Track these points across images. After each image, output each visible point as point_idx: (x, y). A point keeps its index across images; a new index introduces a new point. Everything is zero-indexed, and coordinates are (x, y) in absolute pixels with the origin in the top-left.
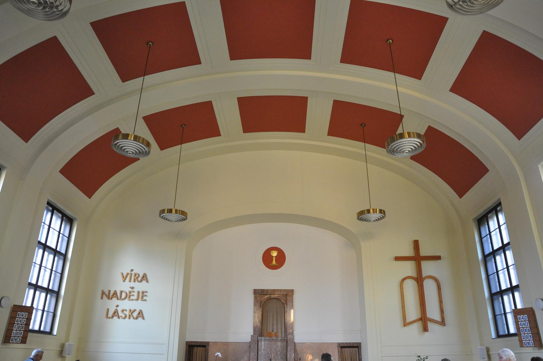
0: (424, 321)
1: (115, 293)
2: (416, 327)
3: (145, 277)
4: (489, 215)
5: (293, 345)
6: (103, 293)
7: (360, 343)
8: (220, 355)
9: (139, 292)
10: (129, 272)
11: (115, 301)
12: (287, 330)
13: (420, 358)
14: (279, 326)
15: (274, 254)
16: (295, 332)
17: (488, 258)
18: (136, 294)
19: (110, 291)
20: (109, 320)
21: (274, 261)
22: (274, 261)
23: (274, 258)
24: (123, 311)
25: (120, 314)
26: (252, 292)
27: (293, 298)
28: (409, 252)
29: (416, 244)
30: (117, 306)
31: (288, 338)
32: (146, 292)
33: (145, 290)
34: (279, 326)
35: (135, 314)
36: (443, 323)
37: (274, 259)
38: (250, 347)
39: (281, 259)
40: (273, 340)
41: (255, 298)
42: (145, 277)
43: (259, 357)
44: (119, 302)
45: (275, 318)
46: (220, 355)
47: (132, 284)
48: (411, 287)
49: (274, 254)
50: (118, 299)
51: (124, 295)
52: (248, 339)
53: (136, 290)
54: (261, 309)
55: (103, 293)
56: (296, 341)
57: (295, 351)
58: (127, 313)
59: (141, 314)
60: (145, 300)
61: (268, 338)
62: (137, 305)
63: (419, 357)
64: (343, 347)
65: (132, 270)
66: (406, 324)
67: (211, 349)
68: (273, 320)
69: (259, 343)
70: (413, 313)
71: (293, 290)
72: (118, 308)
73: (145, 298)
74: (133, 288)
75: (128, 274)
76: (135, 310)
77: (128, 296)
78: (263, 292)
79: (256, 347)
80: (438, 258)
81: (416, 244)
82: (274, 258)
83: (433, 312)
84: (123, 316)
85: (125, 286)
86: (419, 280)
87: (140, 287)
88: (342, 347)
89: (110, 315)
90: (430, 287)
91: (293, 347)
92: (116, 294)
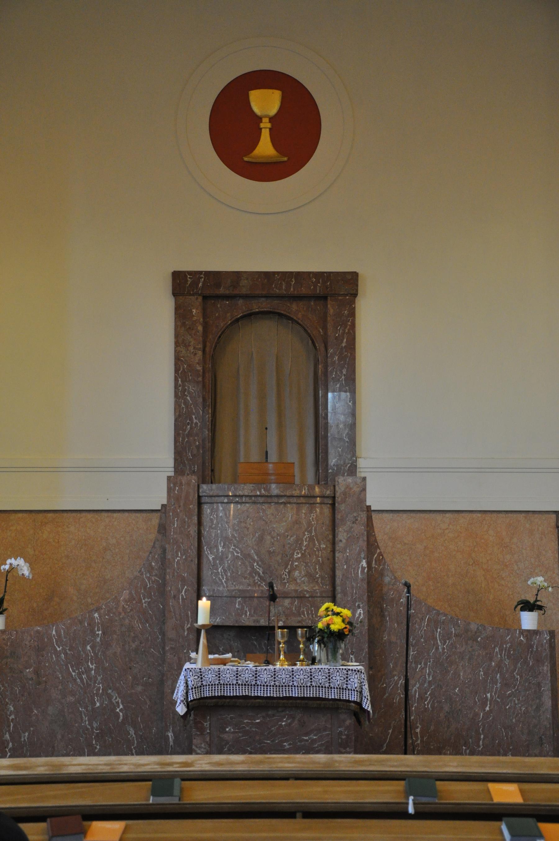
5: (364, 515)
8: (25, 570)
14: (292, 440)
15: (265, 103)
16: (361, 463)
21: (265, 136)
22: (265, 136)
23: (265, 125)
27: (352, 314)
31: (340, 489)
34: (292, 440)
37: (265, 130)
38: (163, 529)
40: (269, 498)
41: (181, 314)
43: (206, 573)
45: (272, 401)
46: (25, 570)
49: (265, 103)
52: (156, 496)
56: (375, 499)
57: (410, 722)
61: (246, 489)
68: (262, 397)
69: (207, 510)
71: (355, 275)
78: (218, 285)
79: (193, 530)
82: (265, 125)
91: (360, 529)
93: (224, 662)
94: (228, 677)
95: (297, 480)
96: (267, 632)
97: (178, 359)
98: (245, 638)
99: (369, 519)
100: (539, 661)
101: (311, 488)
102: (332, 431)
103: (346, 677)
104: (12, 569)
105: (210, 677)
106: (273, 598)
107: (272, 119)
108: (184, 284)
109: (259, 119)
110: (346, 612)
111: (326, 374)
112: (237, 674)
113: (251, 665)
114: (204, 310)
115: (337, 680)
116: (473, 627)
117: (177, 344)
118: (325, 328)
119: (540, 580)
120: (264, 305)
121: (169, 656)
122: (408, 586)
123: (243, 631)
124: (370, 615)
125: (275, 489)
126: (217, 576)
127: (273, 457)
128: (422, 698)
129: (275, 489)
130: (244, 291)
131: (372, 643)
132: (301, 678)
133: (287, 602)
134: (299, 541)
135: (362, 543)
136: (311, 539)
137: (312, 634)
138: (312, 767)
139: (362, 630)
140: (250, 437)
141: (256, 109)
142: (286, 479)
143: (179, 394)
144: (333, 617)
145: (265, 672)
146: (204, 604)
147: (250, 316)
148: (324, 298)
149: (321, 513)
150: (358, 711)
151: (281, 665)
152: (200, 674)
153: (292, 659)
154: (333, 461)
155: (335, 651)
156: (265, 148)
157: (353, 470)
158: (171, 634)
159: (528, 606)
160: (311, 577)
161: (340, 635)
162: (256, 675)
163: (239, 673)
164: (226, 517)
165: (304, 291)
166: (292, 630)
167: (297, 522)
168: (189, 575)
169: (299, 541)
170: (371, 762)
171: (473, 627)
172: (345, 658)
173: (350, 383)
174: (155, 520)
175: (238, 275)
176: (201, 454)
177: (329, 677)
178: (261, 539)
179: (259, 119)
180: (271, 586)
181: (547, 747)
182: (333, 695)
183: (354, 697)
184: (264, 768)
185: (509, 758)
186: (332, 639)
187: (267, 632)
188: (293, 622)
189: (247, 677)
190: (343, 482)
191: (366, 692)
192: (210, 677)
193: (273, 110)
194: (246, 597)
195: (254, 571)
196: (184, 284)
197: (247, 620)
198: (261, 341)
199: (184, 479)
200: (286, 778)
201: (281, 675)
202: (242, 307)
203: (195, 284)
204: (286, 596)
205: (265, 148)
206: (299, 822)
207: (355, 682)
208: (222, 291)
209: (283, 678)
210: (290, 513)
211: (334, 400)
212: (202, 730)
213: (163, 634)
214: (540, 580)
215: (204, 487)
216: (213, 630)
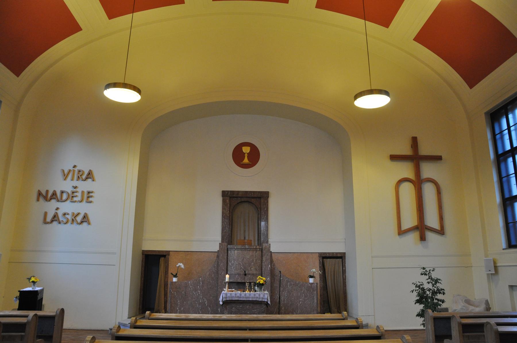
0: (421, 229)
1: (54, 194)
2: (415, 236)
3: (90, 175)
4: (509, 107)
6: (40, 194)
7: (344, 254)
8: (183, 266)
9: (83, 192)
10: (72, 168)
11: (54, 204)
12: (261, 239)
13: (424, 271)
15: (246, 150)
16: (269, 240)
17: (501, 158)
18: (79, 194)
19: (47, 191)
20: (47, 225)
23: (246, 155)
24: (65, 214)
25: (61, 218)
26: (221, 193)
27: (268, 202)
28: (406, 150)
29: (415, 141)
30: (57, 209)
31: (264, 247)
32: (92, 192)
33: (90, 190)
35: (79, 219)
36: (441, 232)
37: (246, 156)
38: (218, 257)
39: (255, 156)
40: (245, 249)
41: (224, 201)
42: (90, 175)
43: (229, 268)
44: (59, 205)
46: (183, 266)
47: (75, 183)
48: (408, 191)
49: (246, 150)
50: (58, 201)
51: (65, 196)
53: (79, 190)
54: (277, 272)
55: (40, 194)
56: (273, 249)
57: (272, 261)
58: (69, 217)
59: (85, 219)
60: (91, 202)
61: (239, 247)
62: (81, 208)
63: (424, 269)
64: (324, 257)
65: (75, 166)
66: (401, 232)
67: (172, 259)
69: (229, 252)
70: (410, 220)
71: (268, 192)
72: (58, 212)
73: (90, 199)
74: (75, 187)
75: (70, 171)
76: (78, 214)
77: (71, 197)
78: (234, 194)
79: (226, 257)
80: (438, 158)
81: (415, 141)
82: (246, 155)
83: (432, 220)
84: (65, 221)
85: (67, 186)
86: (418, 182)
87: (84, 186)
88: (324, 258)
89: (49, 219)
90: (429, 190)
91: (269, 257)
92: (56, 194)
93: (232, 291)
94: (233, 295)
95: (253, 244)
96: (244, 284)
97: (223, 213)
98: (239, 285)
99: (271, 255)
100: (314, 291)
101: (256, 246)
102: (262, 232)
103: (264, 295)
104: (179, 266)
105: (229, 295)
106: (245, 275)
107: (248, 154)
108: (225, 194)
109: (245, 154)
110: (264, 279)
111: (261, 217)
112: (236, 294)
113: (239, 292)
114: (230, 201)
115: (262, 296)
116: (297, 282)
117: (223, 209)
118: (260, 205)
119: (314, 270)
120: (245, 199)
121: (219, 290)
122: (280, 272)
123: (238, 283)
124: (271, 279)
125: (247, 247)
126: (232, 269)
127: (247, 238)
128: (284, 301)
129: (247, 247)
130: (240, 196)
131: (271, 287)
132: (252, 295)
133: (249, 276)
134: (253, 260)
135: (269, 261)
136: (256, 260)
137: (255, 284)
138: (252, 318)
139: (269, 283)
140: (239, 235)
141: (244, 151)
142: (250, 244)
143: (223, 222)
144: (261, 280)
145: (243, 294)
146: (227, 276)
147: (241, 202)
148: (260, 198)
149: (259, 253)
150: (267, 304)
151: (247, 292)
152: (226, 294)
153: (250, 291)
154: (262, 240)
155: (261, 289)
156: (246, 161)
157: (267, 242)
158: (220, 284)
159: (311, 277)
160: (256, 269)
161: (263, 284)
162: (241, 294)
163: (236, 294)
164: (234, 254)
165: (255, 196)
166: (250, 283)
167: (253, 255)
168: (224, 268)
169: (253, 260)
170: (267, 317)
171: (297, 282)
172: (264, 290)
173: (267, 220)
174: (216, 254)
175: (238, 192)
176: (228, 238)
177: (259, 295)
178: (243, 259)
179: (245, 154)
180: (245, 272)
181: (315, 312)
182: (260, 300)
183: (266, 300)
184: (240, 318)
185: (306, 315)
186: (260, 285)
187: (244, 284)
188: (251, 281)
189: (238, 295)
190: (264, 245)
191: (269, 299)
192: (229, 295)
193: (248, 151)
194: (239, 274)
195: (241, 268)
196: (225, 194)
197: (239, 281)
198: (245, 209)
199: (224, 244)
200: (246, 321)
201: (247, 294)
202: (239, 200)
203: (228, 194)
204: (249, 274)
205: (246, 161)
206: (248, 331)
207: (266, 296)
208: (234, 196)
209: (248, 295)
210: (251, 253)
211: (263, 223)
212: (226, 308)
213: (218, 284)
214: (314, 270)
215: (229, 246)
216: (230, 283)
